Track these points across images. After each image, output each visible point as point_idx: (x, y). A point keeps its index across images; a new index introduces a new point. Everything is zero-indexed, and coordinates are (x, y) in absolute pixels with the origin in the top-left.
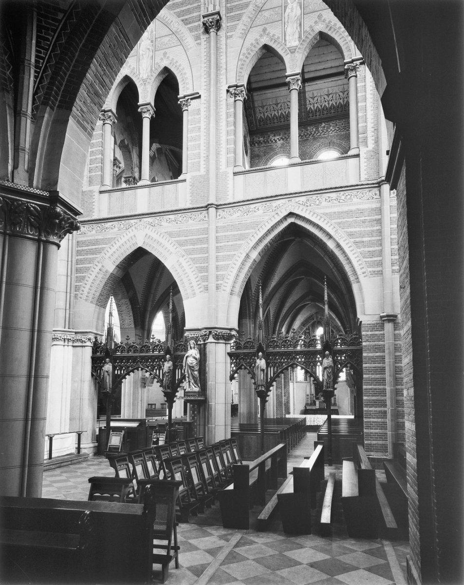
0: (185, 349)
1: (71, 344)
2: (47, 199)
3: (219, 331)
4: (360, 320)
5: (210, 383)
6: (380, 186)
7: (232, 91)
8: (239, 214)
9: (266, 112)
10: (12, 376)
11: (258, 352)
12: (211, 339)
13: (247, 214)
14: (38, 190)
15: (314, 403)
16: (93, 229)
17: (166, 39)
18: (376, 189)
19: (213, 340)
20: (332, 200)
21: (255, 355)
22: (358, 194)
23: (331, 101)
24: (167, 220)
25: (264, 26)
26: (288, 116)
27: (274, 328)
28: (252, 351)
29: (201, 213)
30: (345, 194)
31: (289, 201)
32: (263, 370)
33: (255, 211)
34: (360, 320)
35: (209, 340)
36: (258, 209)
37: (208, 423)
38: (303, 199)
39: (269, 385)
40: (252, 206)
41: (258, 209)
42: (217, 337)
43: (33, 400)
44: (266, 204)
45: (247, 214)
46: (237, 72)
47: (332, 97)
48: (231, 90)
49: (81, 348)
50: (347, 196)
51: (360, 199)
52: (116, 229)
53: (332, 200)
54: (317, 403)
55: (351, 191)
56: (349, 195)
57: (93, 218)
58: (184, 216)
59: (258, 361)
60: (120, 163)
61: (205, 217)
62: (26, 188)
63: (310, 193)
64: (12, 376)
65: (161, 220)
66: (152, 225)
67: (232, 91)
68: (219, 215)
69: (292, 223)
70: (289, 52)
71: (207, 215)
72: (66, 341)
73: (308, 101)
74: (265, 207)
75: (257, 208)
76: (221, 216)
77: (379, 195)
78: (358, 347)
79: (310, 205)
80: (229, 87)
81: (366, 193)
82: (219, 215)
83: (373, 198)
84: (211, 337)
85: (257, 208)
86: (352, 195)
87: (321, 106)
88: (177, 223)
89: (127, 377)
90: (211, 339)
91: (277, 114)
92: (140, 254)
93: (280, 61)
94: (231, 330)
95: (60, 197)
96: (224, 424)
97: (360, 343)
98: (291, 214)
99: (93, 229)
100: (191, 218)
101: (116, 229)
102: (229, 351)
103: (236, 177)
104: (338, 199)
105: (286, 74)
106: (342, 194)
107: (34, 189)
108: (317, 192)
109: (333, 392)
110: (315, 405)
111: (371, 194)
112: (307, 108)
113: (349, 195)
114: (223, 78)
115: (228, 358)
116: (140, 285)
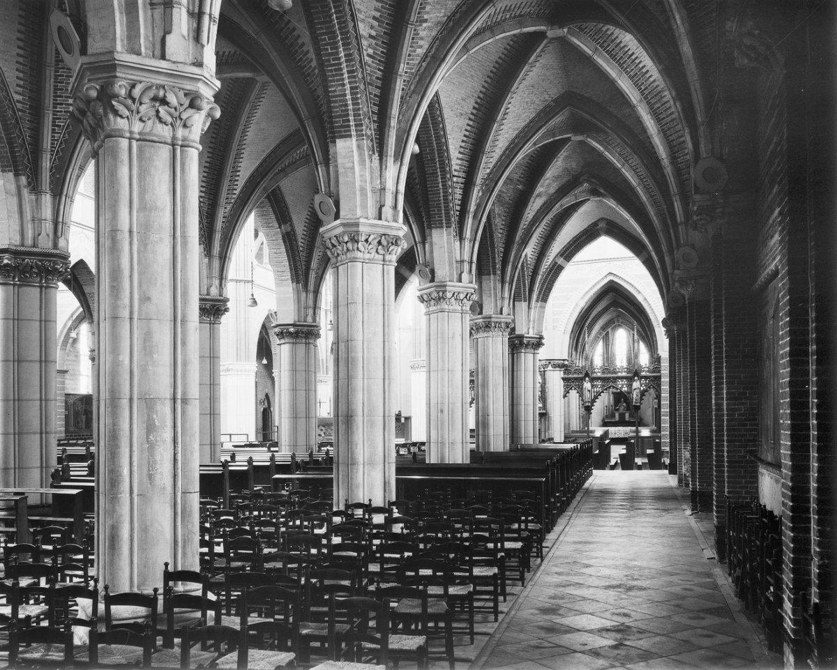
3: (556, 362)
5: (549, 401)
10: (290, 390)
11: (634, 376)
12: (550, 368)
15: (613, 415)
19: (552, 369)
21: (582, 379)
28: (580, 376)
32: (589, 391)
35: (549, 369)
37: (548, 430)
38: (620, 263)
39: (593, 401)
42: (555, 366)
54: (617, 415)
59: (585, 384)
64: (290, 390)
78: (658, 374)
84: (550, 366)
89: (597, 400)
90: (550, 368)
93: (272, 333)
94: (564, 360)
97: (659, 371)
98: (610, 273)
102: (562, 376)
109: (640, 406)
110: (614, 417)
115: (562, 381)
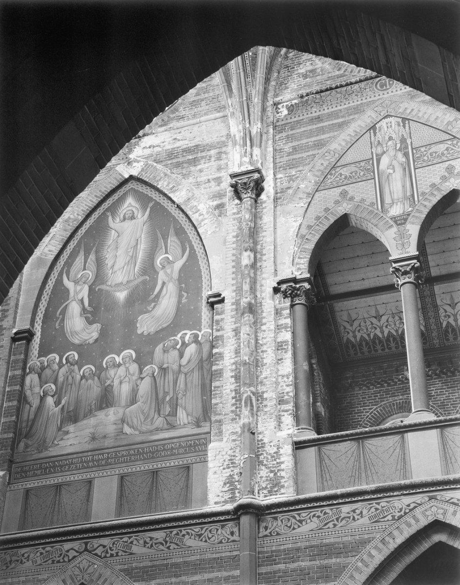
6: (238, 518)
7: (286, 289)
8: (314, 524)
9: (359, 331)
13: (335, 525)
17: (442, 148)
18: (230, 524)
20: (156, 544)
22: (203, 532)
23: (386, 327)
24: (145, 542)
25: (342, 188)
26: (400, 339)
29: (223, 527)
30: (181, 531)
31: (431, 498)
33: (354, 519)
36: (361, 512)
40: (346, 509)
44: (44, 548)
45: (335, 525)
46: (288, 255)
47: (387, 321)
48: (284, 287)
50: (184, 535)
51: (206, 541)
52: (365, 521)
53: (156, 544)
56: (188, 533)
58: (184, 532)
61: (232, 533)
65: (132, 543)
67: (286, 289)
69: (440, 542)
70: (392, 223)
71: (236, 530)
73: (441, 311)
74: (41, 554)
75: (358, 512)
76: (269, 531)
77: (237, 534)
80: (279, 283)
81: (217, 530)
82: (266, 528)
83: (228, 539)
85: (358, 512)
86: (192, 535)
87: (369, 335)
88: (168, 548)
91: (453, 323)
98: (437, 526)
100: (200, 536)
101: (365, 521)
103: (297, 451)
105: (390, 258)
106: (175, 532)
108: (218, 518)
112: (441, 324)
114: (267, 265)
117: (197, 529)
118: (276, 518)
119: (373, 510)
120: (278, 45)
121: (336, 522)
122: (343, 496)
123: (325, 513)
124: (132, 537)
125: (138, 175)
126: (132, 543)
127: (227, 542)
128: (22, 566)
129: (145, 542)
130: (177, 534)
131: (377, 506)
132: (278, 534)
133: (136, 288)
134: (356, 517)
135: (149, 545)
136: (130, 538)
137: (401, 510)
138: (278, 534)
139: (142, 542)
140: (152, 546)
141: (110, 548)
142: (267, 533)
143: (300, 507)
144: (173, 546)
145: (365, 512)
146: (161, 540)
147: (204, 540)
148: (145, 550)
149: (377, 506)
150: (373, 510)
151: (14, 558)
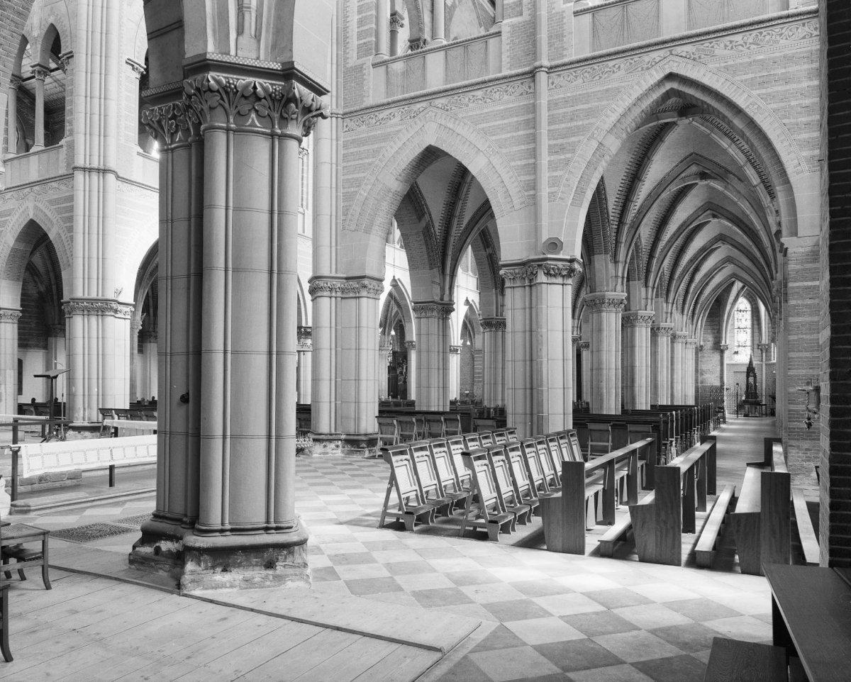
0: (429, 152)
1: (339, 294)
2: (280, 75)
4: (785, 247)
13: (600, 77)
14: (275, 64)
16: (363, 122)
20: (735, 46)
22: (784, 31)
27: (647, 267)
33: (614, 72)
34: (785, 247)
36: (619, 67)
40: (611, 64)
41: (619, 67)
43: (313, 313)
45: (600, 77)
49: (355, 300)
51: (787, 39)
55: (770, 28)
56: (769, 34)
57: (566, 60)
58: (496, 90)
60: (403, 19)
62: (250, 62)
63: (779, 22)
65: (713, 47)
66: (444, 109)
68: (553, 83)
72: (334, 291)
79: (700, 57)
82: (553, 83)
83: (811, 34)
86: (772, 35)
88: (486, 102)
92: (431, 155)
95: (297, 70)
96: (562, 412)
98: (671, 77)
99: (363, 122)
104: (746, 43)
106: (489, 91)
107: (260, 61)
111: (806, 28)
113: (769, 34)
116: (436, 208)
117: (504, 86)
118: (559, 75)
119: (628, 63)
120: (160, 190)
121: (601, 75)
122: (633, 49)
123: (594, 69)
124: (712, 42)
125: (150, 188)
126: (713, 47)
127: (811, 37)
128: (613, 75)
129: (726, 46)
130: (491, 92)
131: (631, 61)
132: (561, 87)
133: (686, 449)
134: (615, 70)
135: (729, 48)
136: (710, 43)
137: (649, 62)
138: (561, 87)
139: (722, 45)
140: (732, 48)
141: (693, 53)
142: (347, 129)
143: (664, 46)
144: (488, 100)
145: (622, 66)
146: (742, 42)
147: (784, 38)
148: (727, 52)
149: (631, 61)
150: (628, 63)
151: (606, 70)
